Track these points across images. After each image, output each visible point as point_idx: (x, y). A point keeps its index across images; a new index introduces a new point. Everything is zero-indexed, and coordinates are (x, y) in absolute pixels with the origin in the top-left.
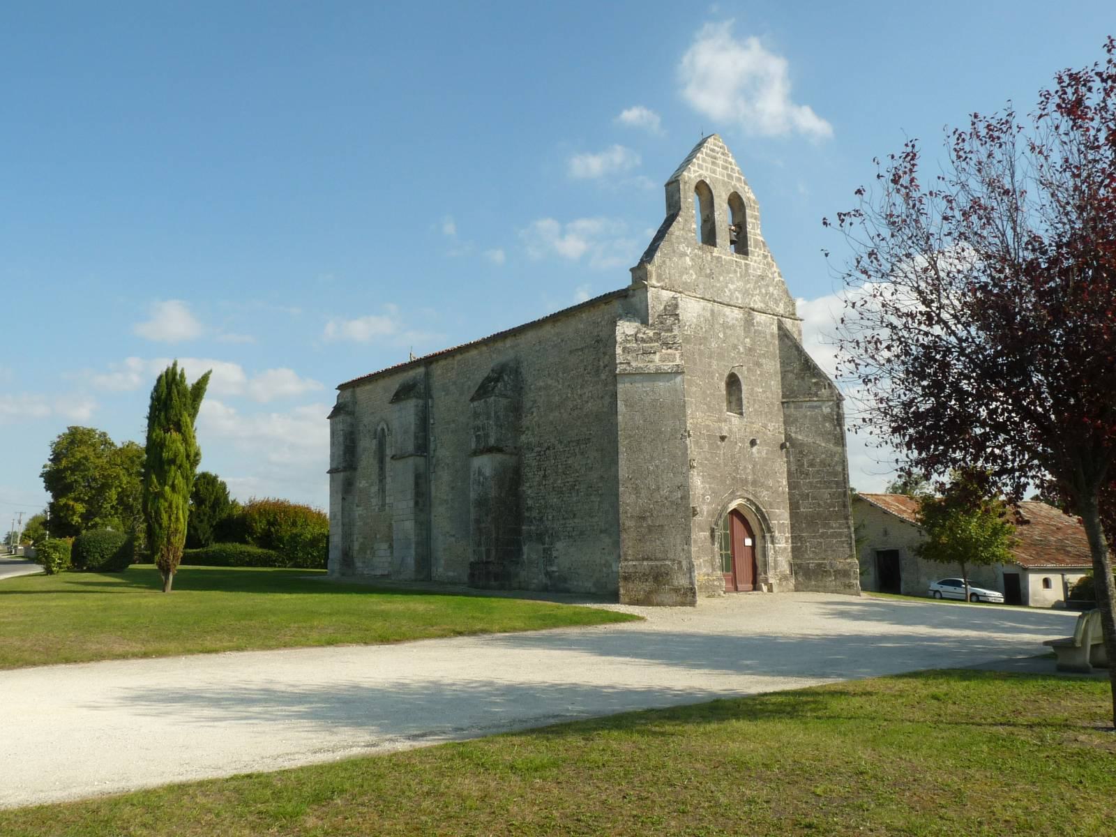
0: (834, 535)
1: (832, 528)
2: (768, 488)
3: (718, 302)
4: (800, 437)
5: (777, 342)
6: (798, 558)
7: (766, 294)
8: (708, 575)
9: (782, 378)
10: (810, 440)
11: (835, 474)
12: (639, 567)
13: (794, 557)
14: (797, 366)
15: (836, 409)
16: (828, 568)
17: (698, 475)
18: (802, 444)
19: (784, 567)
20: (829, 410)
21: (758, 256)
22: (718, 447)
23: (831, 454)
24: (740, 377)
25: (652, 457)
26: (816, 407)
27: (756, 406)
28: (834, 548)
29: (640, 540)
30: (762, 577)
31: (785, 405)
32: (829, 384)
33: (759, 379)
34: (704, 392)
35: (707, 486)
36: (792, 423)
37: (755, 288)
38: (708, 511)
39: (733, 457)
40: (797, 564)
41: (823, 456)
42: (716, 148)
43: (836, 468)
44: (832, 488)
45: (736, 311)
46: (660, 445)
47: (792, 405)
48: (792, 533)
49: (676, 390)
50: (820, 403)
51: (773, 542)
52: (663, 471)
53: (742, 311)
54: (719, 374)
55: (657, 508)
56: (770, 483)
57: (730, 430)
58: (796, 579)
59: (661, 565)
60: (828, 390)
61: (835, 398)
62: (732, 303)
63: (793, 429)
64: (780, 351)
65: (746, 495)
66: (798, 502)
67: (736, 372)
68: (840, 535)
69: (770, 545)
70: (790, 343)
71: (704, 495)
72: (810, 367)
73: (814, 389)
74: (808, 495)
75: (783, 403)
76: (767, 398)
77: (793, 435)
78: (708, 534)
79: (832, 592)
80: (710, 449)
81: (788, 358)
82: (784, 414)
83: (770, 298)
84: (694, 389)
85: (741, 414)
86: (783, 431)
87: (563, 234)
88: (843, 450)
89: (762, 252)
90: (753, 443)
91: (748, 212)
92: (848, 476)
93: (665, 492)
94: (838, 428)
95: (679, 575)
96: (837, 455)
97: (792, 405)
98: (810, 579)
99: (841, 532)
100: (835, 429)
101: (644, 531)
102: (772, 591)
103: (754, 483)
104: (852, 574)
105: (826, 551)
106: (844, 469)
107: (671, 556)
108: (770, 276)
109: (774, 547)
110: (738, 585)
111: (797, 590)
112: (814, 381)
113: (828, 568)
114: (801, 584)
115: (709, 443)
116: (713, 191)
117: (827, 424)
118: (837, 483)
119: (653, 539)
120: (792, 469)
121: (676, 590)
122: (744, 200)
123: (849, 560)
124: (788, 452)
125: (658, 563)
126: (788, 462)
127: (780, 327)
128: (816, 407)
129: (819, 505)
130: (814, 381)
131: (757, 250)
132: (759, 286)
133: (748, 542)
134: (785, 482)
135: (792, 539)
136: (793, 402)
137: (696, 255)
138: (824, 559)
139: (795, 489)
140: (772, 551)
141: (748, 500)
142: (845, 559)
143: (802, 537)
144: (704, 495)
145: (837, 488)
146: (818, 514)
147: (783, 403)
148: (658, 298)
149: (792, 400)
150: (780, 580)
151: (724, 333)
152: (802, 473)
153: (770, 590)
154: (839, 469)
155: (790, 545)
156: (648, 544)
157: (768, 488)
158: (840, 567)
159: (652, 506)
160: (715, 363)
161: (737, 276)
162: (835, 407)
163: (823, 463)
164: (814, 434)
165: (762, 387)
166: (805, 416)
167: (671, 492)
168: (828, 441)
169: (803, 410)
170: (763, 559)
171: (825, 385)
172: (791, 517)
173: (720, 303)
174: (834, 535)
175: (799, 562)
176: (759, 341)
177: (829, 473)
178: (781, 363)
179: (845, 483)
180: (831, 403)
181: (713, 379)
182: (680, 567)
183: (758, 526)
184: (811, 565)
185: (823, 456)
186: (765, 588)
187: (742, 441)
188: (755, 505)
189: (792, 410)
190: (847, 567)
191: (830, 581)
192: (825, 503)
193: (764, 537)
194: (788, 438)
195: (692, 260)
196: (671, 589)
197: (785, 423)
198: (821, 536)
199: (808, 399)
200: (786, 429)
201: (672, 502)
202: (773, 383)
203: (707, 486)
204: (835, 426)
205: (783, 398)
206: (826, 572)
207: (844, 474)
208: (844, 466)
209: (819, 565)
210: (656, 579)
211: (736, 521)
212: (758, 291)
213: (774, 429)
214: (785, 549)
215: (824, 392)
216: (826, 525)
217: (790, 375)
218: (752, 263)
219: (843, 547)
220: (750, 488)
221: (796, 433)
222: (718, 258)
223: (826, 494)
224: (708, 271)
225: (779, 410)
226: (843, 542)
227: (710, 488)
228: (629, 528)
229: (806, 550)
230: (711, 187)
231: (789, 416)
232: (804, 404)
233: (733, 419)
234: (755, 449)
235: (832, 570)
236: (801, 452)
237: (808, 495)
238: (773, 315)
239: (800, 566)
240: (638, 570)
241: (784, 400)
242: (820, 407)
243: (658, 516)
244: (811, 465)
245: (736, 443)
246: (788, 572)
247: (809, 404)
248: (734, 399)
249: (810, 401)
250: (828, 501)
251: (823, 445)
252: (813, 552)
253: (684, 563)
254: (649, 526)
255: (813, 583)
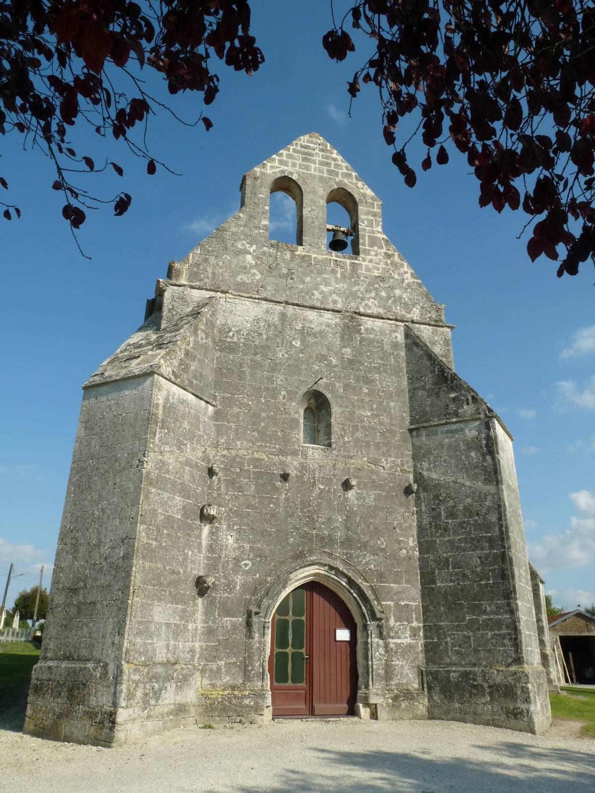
0: (487, 625)
1: (485, 612)
2: (376, 551)
3: (293, 304)
4: (434, 476)
5: (403, 354)
6: (434, 663)
7: (389, 298)
8: (233, 688)
9: (410, 399)
10: (449, 479)
11: (488, 527)
12: (54, 670)
13: (429, 660)
14: (429, 380)
15: (484, 431)
16: (480, 680)
17: (229, 528)
18: (438, 486)
19: (407, 674)
20: (474, 433)
21: (376, 255)
22: (276, 489)
23: (480, 497)
24: (329, 396)
25: (100, 496)
26: (457, 431)
27: (359, 434)
28: (490, 647)
29: (66, 626)
30: (361, 693)
31: (415, 433)
32: (473, 397)
33: (367, 399)
34: (256, 416)
35: (247, 546)
36: (424, 456)
37: (368, 291)
38: (243, 585)
39: (305, 504)
40: (431, 673)
41: (469, 500)
42: (312, 145)
43: (489, 517)
44: (483, 549)
45: (328, 315)
46: (111, 478)
47: (423, 432)
48: (425, 621)
49: (143, 399)
50: (462, 425)
51: (381, 636)
52: (108, 517)
53: (338, 315)
54: (288, 392)
55: (94, 574)
56: (382, 542)
57: (303, 467)
58: (430, 698)
59: (81, 669)
60: (472, 406)
61: (482, 416)
62: (328, 307)
63: (425, 465)
64: (408, 363)
65: (328, 560)
66: (433, 573)
67: (321, 390)
68: (498, 624)
69: (376, 640)
70: (421, 352)
71: (237, 560)
72: (446, 379)
73: (453, 407)
74: (447, 560)
75: (411, 431)
76: (381, 424)
77: (425, 473)
78: (240, 620)
79: (487, 724)
80: (257, 489)
81: (418, 372)
82: (413, 445)
83: (394, 302)
84: (236, 410)
85: (330, 445)
86: (412, 470)
87: (580, 390)
88: (498, 489)
89: (384, 250)
90: (347, 486)
91: (360, 208)
92: (507, 528)
93: (105, 550)
94: (488, 458)
95: (100, 687)
96: (489, 498)
97: (423, 432)
98: (450, 698)
99: (500, 620)
100: (484, 459)
101: (73, 610)
102: (376, 719)
103: (347, 542)
104: (519, 692)
105: (476, 651)
106: (500, 519)
107: (97, 654)
108: (396, 276)
109: (386, 646)
110: (315, 705)
111: (431, 717)
112: (452, 395)
113: (480, 680)
114: (439, 707)
115: (257, 484)
116: (303, 188)
117: (473, 454)
118: (490, 540)
119: (80, 625)
120: (424, 522)
121: (91, 715)
122: (356, 196)
123: (513, 668)
124: (418, 498)
125: (78, 665)
126: (419, 513)
127: (408, 335)
128: (457, 431)
129: (464, 575)
130: (452, 395)
131: (376, 248)
132: (376, 289)
133: (343, 635)
134: (412, 542)
135: (425, 631)
136: (424, 427)
137: (264, 253)
138: (474, 665)
139: (427, 552)
140: (382, 651)
141: (331, 568)
142: (509, 665)
143: (441, 627)
144: (237, 560)
145: (491, 547)
146: (462, 590)
147: (411, 431)
148: (183, 299)
149: (421, 425)
150: (395, 698)
151: (303, 342)
152: (438, 527)
153: (374, 716)
154: (493, 518)
155: (422, 641)
156: (74, 632)
157: (376, 551)
158: (498, 679)
159: (87, 571)
160: (281, 377)
161: (336, 278)
162: (483, 429)
163: (468, 510)
164: (454, 469)
165: (372, 409)
166: (442, 445)
167: (113, 548)
168: (475, 477)
169: (439, 437)
170: (365, 662)
171: (468, 400)
172: (423, 596)
173: (297, 305)
174: (487, 625)
175: (434, 668)
176: (370, 351)
177: (478, 526)
178: (409, 379)
179: (503, 540)
180: (477, 423)
181: (275, 398)
182: (105, 674)
183: (358, 611)
184: (452, 674)
185: (469, 500)
186: (364, 712)
187: (327, 481)
188: (346, 576)
189: (424, 439)
190: (510, 679)
191: (483, 704)
192: (473, 572)
193: (365, 627)
194: (419, 478)
195: (257, 258)
196: (86, 713)
197: (415, 457)
198: (469, 627)
199: (444, 421)
200: (415, 467)
201: (111, 565)
202: (392, 404)
203: (247, 546)
204: (484, 455)
205: (411, 424)
206: (475, 687)
207: (502, 526)
208: (500, 513)
209: (465, 675)
210: (71, 696)
211: (318, 599)
212: (373, 294)
213: (397, 465)
214: (410, 646)
215: (468, 409)
216: (476, 609)
217: (420, 393)
218: (363, 263)
219: (504, 645)
220: (338, 551)
221: (429, 470)
222: (303, 258)
223: (474, 558)
224: (285, 271)
225: (404, 440)
226: (503, 637)
227: (252, 549)
228: (58, 605)
229: (447, 649)
230: (300, 183)
231: (420, 448)
232: (440, 429)
233: (310, 452)
234: (351, 494)
235: (486, 685)
236: (436, 497)
237: (447, 560)
238: (396, 320)
239: (435, 676)
240: (53, 677)
241: (413, 427)
242: (462, 430)
243: (92, 587)
244: (452, 515)
245: (314, 484)
246: (416, 686)
247: (446, 428)
248: (322, 426)
249: (447, 423)
250: (478, 569)
251: (468, 483)
252: (458, 653)
253: (111, 668)
254: (80, 602)
255: (457, 705)
